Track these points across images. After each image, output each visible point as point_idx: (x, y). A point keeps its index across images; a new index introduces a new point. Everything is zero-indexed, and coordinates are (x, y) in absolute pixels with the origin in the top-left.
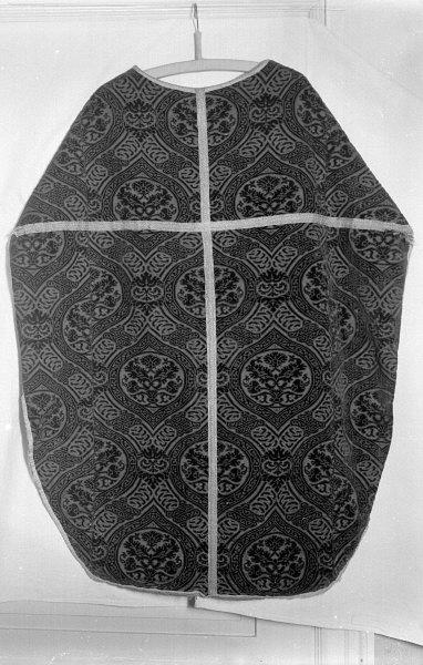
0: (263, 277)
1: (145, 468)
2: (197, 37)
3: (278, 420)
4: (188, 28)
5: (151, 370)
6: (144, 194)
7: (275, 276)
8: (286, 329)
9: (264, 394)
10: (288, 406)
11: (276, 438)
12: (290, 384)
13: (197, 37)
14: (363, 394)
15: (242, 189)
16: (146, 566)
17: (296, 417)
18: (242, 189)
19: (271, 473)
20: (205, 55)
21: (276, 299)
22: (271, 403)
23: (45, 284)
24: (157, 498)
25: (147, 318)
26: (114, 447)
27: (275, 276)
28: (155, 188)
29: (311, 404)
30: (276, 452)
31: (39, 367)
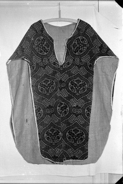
0: (47, 107)
1: (78, 63)
2: (60, 12)
3: (78, 97)
4: (57, 7)
5: (77, 46)
6: (76, 133)
7: (78, 108)
8: (28, 45)
9: (72, 140)
10: (56, 143)
11: (77, 102)
12: (63, 112)
13: (60, 12)
14: (73, 80)
15: (87, 108)
16: (77, 89)
17: (82, 97)
18: (87, 108)
19: (84, 30)
20: (62, 17)
21: (62, 88)
22: (86, 47)
23: (78, 149)
24: (77, 120)
25: (77, 104)
26: (76, 39)
27: (78, 107)
28: (75, 42)
29: (37, 55)
30: (76, 107)
31: (76, 121)
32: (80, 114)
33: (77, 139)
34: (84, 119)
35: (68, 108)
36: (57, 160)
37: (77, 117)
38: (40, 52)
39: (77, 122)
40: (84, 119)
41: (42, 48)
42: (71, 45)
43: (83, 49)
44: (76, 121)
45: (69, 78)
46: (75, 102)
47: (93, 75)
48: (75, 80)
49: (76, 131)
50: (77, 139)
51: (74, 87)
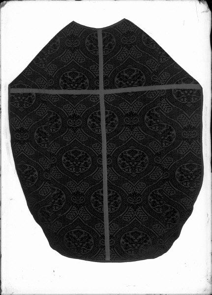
24: (74, 57)
30: (133, 195)
32: (80, 127)
33: (190, 94)
34: (175, 188)
35: (60, 120)
36: (166, 173)
37: (73, 53)
38: (144, 166)
39: (132, 58)
40: (175, 188)
41: (137, 162)
42: (137, 229)
43: (186, 182)
44: (189, 117)
45: (118, 150)
46: (131, 188)
47: (101, 142)
48: (186, 164)
49: (76, 153)
50: (190, 94)
51: (71, 163)
